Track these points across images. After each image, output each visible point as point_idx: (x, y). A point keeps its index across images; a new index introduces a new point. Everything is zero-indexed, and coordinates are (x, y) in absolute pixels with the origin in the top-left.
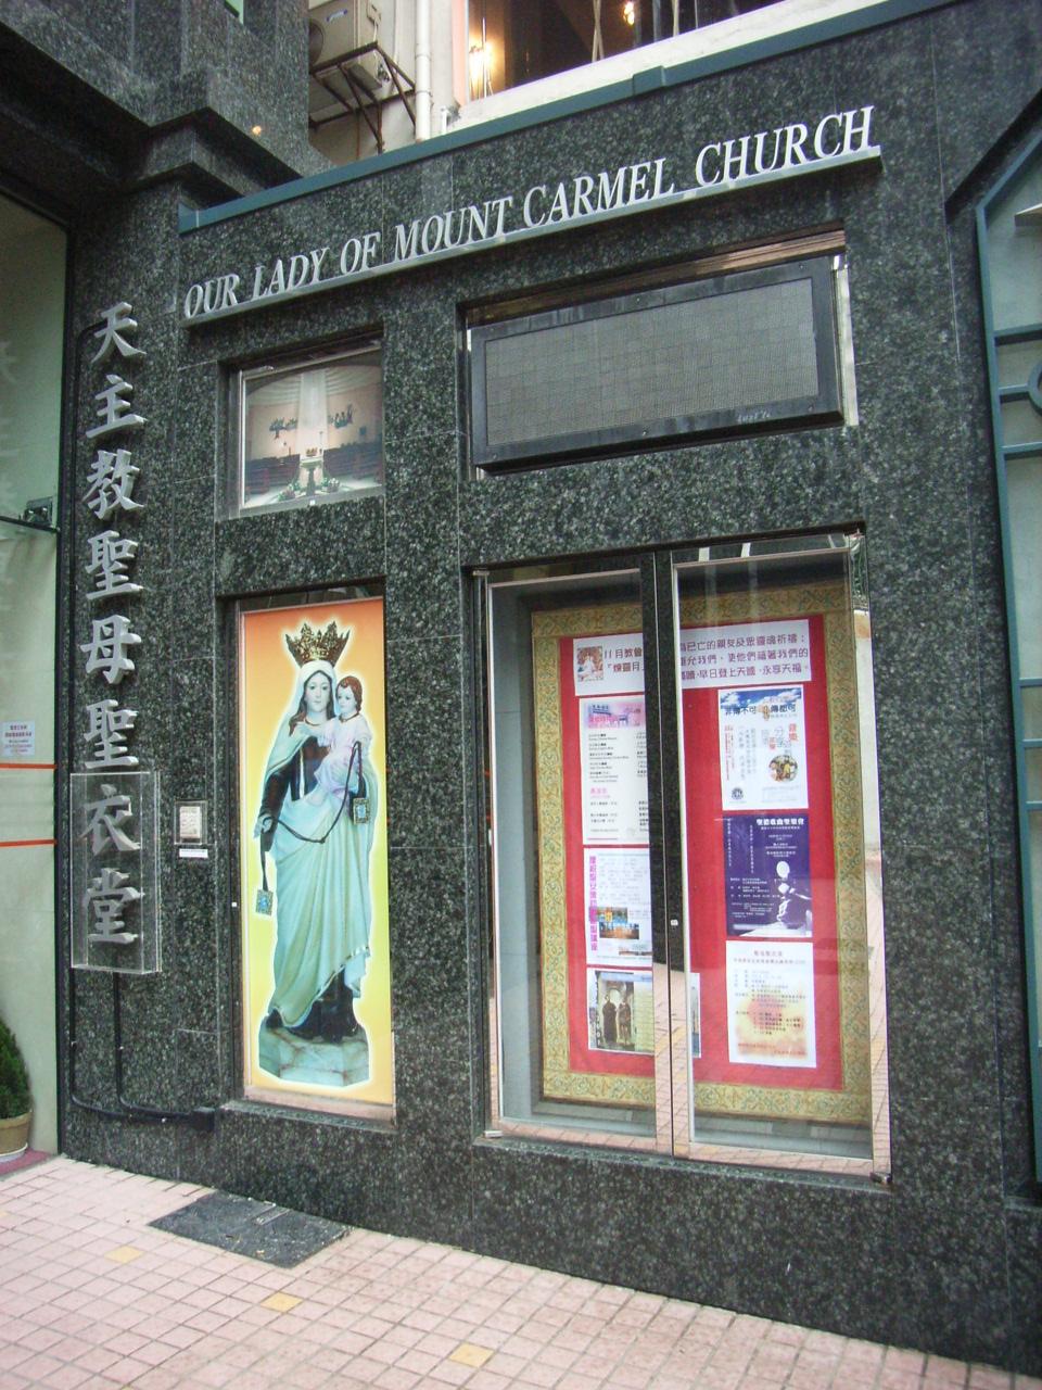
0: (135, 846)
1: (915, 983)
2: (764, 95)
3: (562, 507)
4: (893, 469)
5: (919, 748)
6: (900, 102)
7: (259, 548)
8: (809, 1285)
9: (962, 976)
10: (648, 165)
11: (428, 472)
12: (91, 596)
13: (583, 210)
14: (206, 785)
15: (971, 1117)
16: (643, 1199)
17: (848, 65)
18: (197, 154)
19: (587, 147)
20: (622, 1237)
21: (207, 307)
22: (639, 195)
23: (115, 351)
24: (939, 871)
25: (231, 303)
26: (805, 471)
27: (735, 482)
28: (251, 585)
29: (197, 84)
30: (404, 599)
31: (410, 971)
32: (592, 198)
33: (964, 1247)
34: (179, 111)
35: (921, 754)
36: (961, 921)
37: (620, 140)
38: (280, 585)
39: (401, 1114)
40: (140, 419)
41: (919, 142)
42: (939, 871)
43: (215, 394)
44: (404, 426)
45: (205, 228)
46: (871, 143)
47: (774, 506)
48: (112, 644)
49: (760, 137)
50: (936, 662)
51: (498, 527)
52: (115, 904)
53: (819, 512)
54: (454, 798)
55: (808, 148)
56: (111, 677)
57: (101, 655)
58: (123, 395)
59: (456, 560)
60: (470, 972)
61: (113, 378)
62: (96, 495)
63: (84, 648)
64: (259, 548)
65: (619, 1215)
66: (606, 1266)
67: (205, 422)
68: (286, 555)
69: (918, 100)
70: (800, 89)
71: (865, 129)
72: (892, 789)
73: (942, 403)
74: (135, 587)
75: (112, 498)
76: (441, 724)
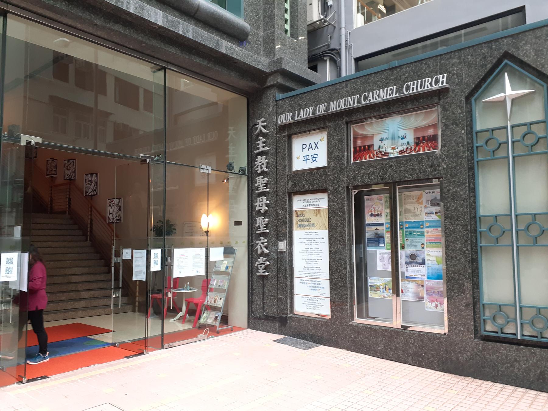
0: (268, 252)
1: (453, 287)
2: (422, 69)
3: (370, 172)
4: (450, 164)
5: (454, 231)
6: (454, 72)
7: (298, 181)
8: (428, 359)
9: (464, 285)
10: (392, 88)
11: (338, 163)
12: (257, 192)
13: (376, 99)
14: (285, 237)
15: (466, 319)
16: (389, 338)
17: (442, 62)
18: (280, 80)
19: (378, 81)
20: (385, 347)
21: (284, 121)
22: (390, 95)
23: (261, 131)
24: (459, 260)
25: (290, 120)
26: (428, 164)
27: (411, 167)
28: (296, 190)
29: (280, 61)
30: (332, 194)
31: (334, 281)
32: (378, 96)
33: (464, 350)
34: (275, 69)
35: (455, 232)
36: (464, 272)
37: (386, 80)
38: (303, 190)
39: (332, 316)
40: (268, 148)
41: (459, 82)
42: (459, 260)
43: (286, 143)
44: (332, 152)
45: (283, 99)
46: (446, 83)
47: (421, 173)
48: (262, 204)
49: (419, 81)
50: (458, 211)
51: (354, 177)
52: (263, 266)
53: (431, 174)
54: (344, 241)
55: (431, 84)
56: (262, 211)
57: (259, 206)
58: (263, 142)
59: (344, 185)
60: (348, 282)
61: (261, 138)
62: (257, 167)
63: (255, 204)
64: (298, 181)
65: (384, 342)
66: (381, 354)
67: (284, 149)
68: (304, 183)
69: (459, 71)
70: (430, 68)
71: (445, 80)
72: (448, 240)
73: (462, 148)
74: (268, 190)
75: (262, 168)
76: (341, 223)
